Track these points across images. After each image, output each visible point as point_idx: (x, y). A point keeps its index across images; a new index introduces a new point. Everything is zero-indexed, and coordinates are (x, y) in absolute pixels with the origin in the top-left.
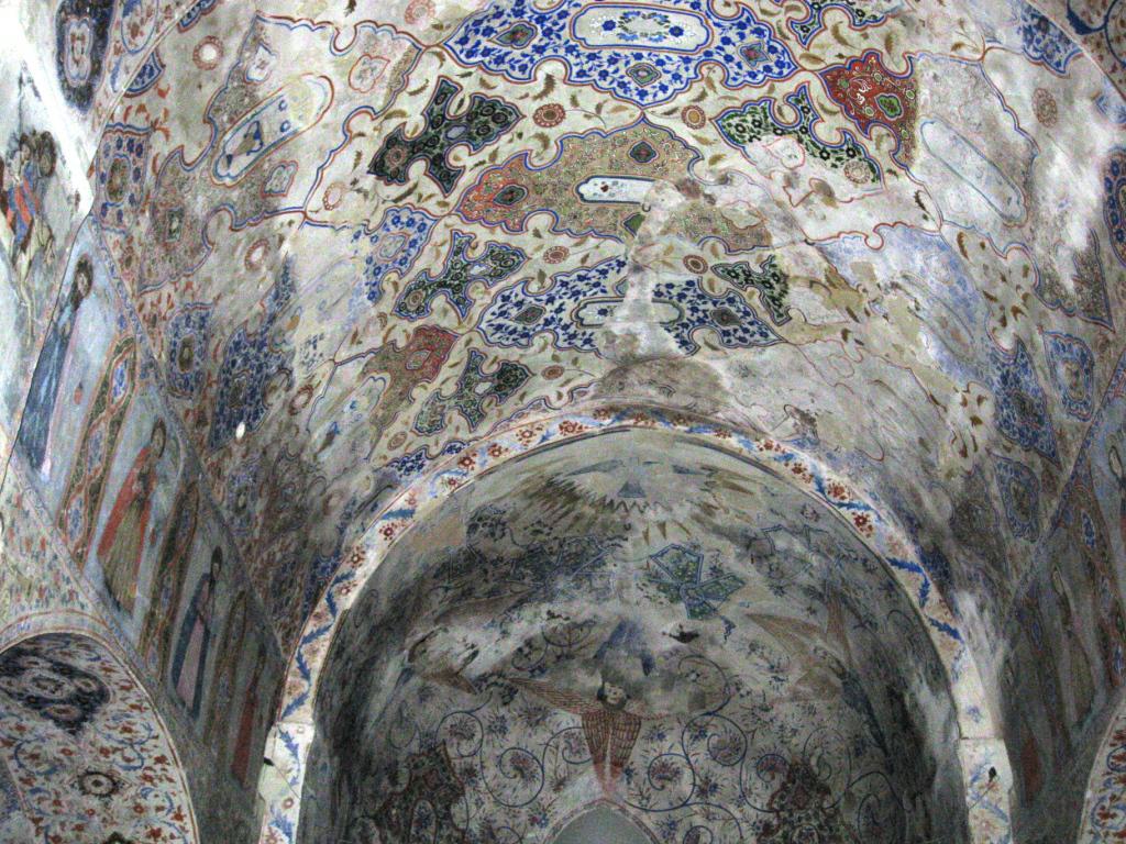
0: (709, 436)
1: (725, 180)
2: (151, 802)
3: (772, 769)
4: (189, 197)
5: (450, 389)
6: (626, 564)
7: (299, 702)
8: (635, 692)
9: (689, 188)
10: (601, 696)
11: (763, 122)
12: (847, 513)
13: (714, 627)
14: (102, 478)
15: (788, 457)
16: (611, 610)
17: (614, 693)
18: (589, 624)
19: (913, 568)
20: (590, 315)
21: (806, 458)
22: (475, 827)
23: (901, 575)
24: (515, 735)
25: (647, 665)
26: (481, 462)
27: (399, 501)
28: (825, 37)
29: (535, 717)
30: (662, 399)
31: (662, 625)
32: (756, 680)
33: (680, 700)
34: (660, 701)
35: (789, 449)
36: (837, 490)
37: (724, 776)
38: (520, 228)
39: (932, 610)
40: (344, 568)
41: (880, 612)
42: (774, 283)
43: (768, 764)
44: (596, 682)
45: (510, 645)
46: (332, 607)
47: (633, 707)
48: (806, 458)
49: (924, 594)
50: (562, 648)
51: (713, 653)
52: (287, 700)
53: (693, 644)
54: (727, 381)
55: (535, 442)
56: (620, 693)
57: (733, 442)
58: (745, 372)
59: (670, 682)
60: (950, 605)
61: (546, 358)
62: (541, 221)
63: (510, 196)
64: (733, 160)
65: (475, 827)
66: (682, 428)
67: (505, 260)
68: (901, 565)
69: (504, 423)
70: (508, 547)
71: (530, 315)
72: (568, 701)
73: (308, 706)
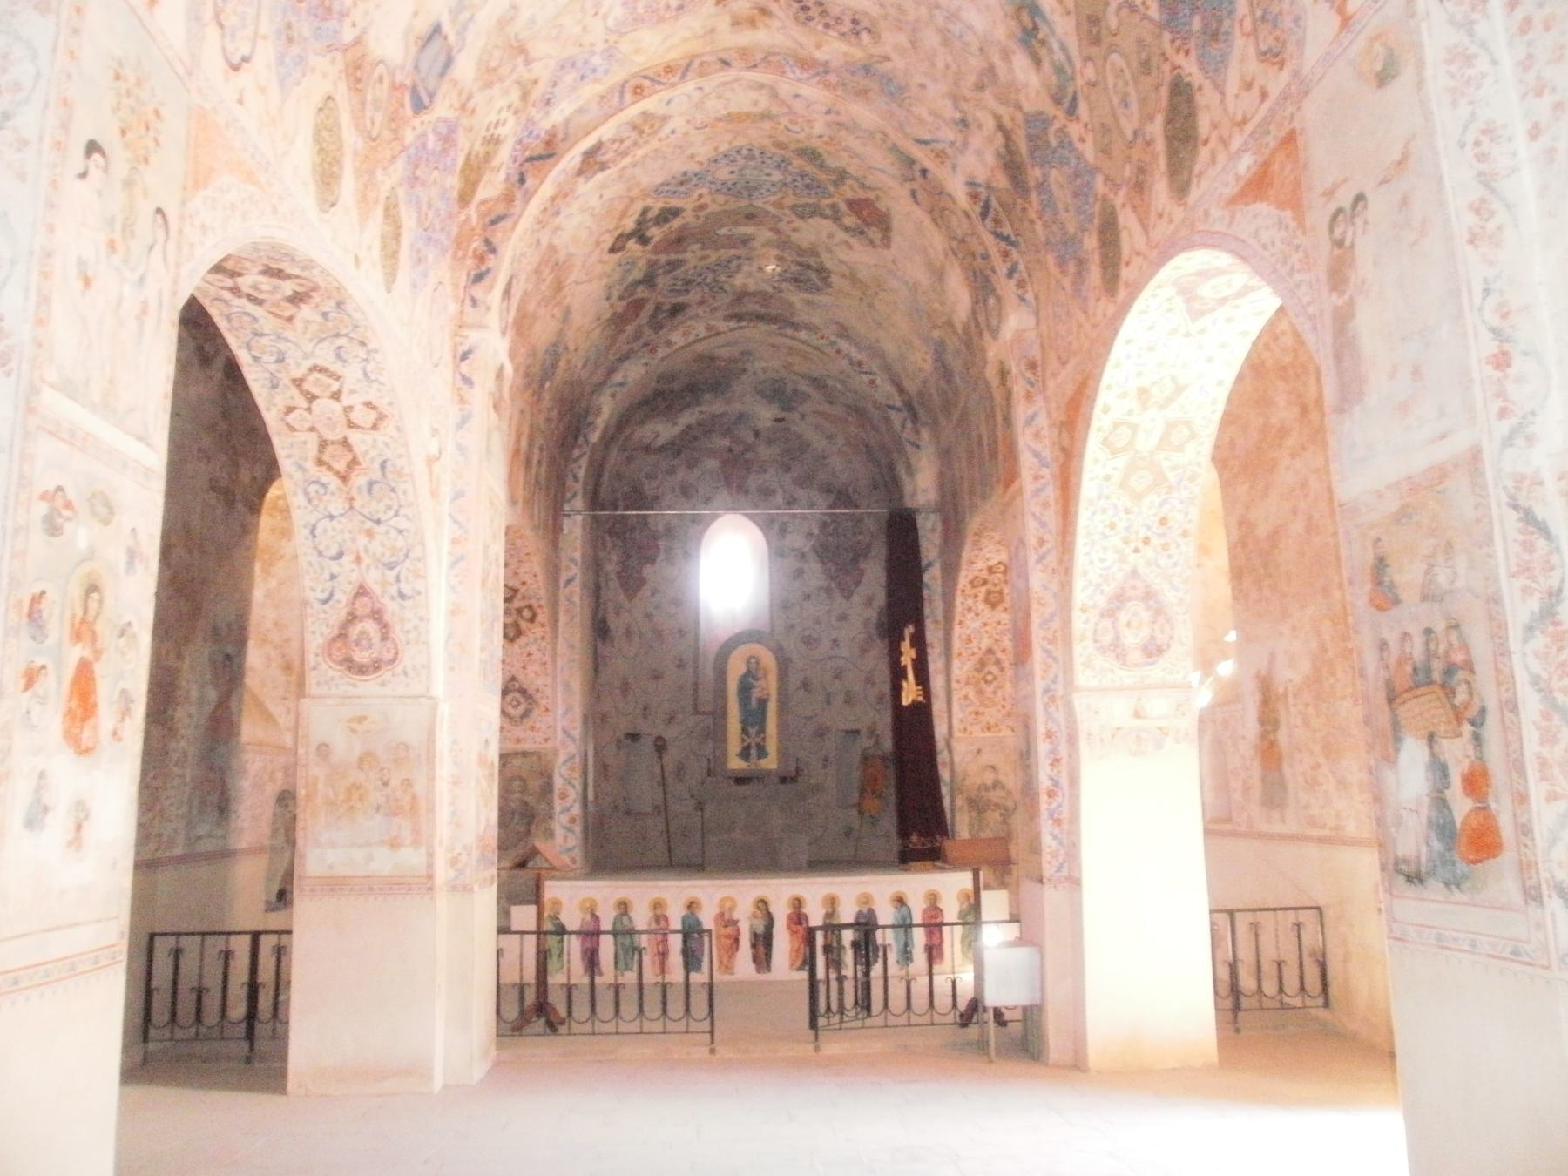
0: (789, 332)
1: (795, 230)
2: (522, 570)
3: (829, 491)
4: (499, 235)
5: (645, 321)
6: (742, 386)
7: (574, 495)
8: (748, 448)
9: (777, 231)
10: (730, 450)
11: (815, 211)
12: (865, 378)
13: (795, 416)
14: (555, 544)
15: (834, 343)
16: (737, 407)
17: (738, 449)
18: (722, 415)
19: (899, 410)
20: (723, 278)
21: (844, 345)
22: (661, 528)
23: (893, 414)
24: (681, 474)
25: (757, 434)
26: (661, 353)
27: (618, 377)
28: (846, 188)
29: (691, 465)
30: (763, 311)
31: (765, 415)
32: (818, 442)
33: (775, 451)
34: (764, 451)
35: (833, 338)
36: (860, 364)
37: (800, 493)
38: (685, 251)
39: (907, 435)
40: (590, 419)
41: (883, 429)
42: (822, 271)
43: (827, 489)
44: (726, 443)
45: (677, 430)
46: (587, 442)
47: (748, 456)
48: (844, 345)
49: (903, 426)
50: (708, 427)
51: (794, 428)
52: (568, 495)
53: (783, 425)
54: (799, 305)
55: (692, 338)
56: (741, 448)
57: (803, 335)
58: (809, 303)
59: (770, 442)
60: (917, 432)
61: (698, 298)
62: (696, 247)
63: (679, 240)
64: (798, 223)
65: (661, 528)
66: (774, 327)
67: (674, 265)
68: (890, 407)
69: (674, 328)
70: (676, 386)
71: (688, 283)
72: (712, 453)
73: (579, 497)
